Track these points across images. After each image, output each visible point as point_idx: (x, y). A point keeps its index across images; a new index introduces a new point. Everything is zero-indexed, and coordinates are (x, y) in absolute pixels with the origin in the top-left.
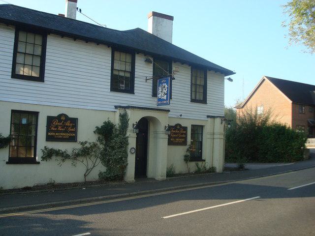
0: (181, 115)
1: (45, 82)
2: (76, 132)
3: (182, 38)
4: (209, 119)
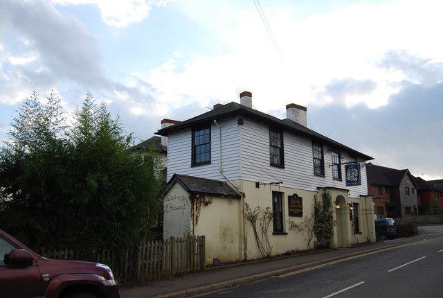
2: (301, 209)
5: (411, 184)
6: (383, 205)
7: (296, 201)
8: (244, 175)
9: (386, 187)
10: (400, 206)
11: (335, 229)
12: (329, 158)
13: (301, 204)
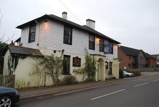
0: (107, 58)
1: (72, 45)
2: (80, 63)
3: (99, 28)
4: (115, 60)
5: (143, 55)
6: (131, 63)
7: (77, 61)
8: (46, 47)
9: (133, 56)
10: (138, 64)
11: (97, 73)
12: (97, 40)
13: (80, 61)
